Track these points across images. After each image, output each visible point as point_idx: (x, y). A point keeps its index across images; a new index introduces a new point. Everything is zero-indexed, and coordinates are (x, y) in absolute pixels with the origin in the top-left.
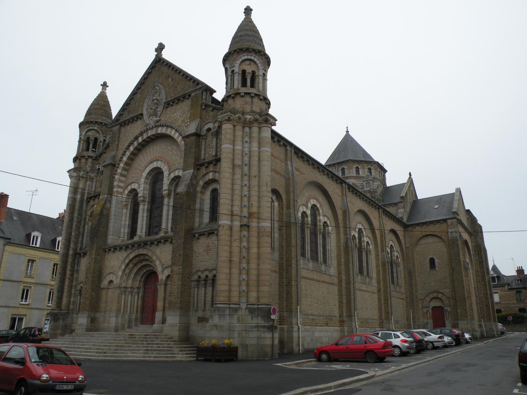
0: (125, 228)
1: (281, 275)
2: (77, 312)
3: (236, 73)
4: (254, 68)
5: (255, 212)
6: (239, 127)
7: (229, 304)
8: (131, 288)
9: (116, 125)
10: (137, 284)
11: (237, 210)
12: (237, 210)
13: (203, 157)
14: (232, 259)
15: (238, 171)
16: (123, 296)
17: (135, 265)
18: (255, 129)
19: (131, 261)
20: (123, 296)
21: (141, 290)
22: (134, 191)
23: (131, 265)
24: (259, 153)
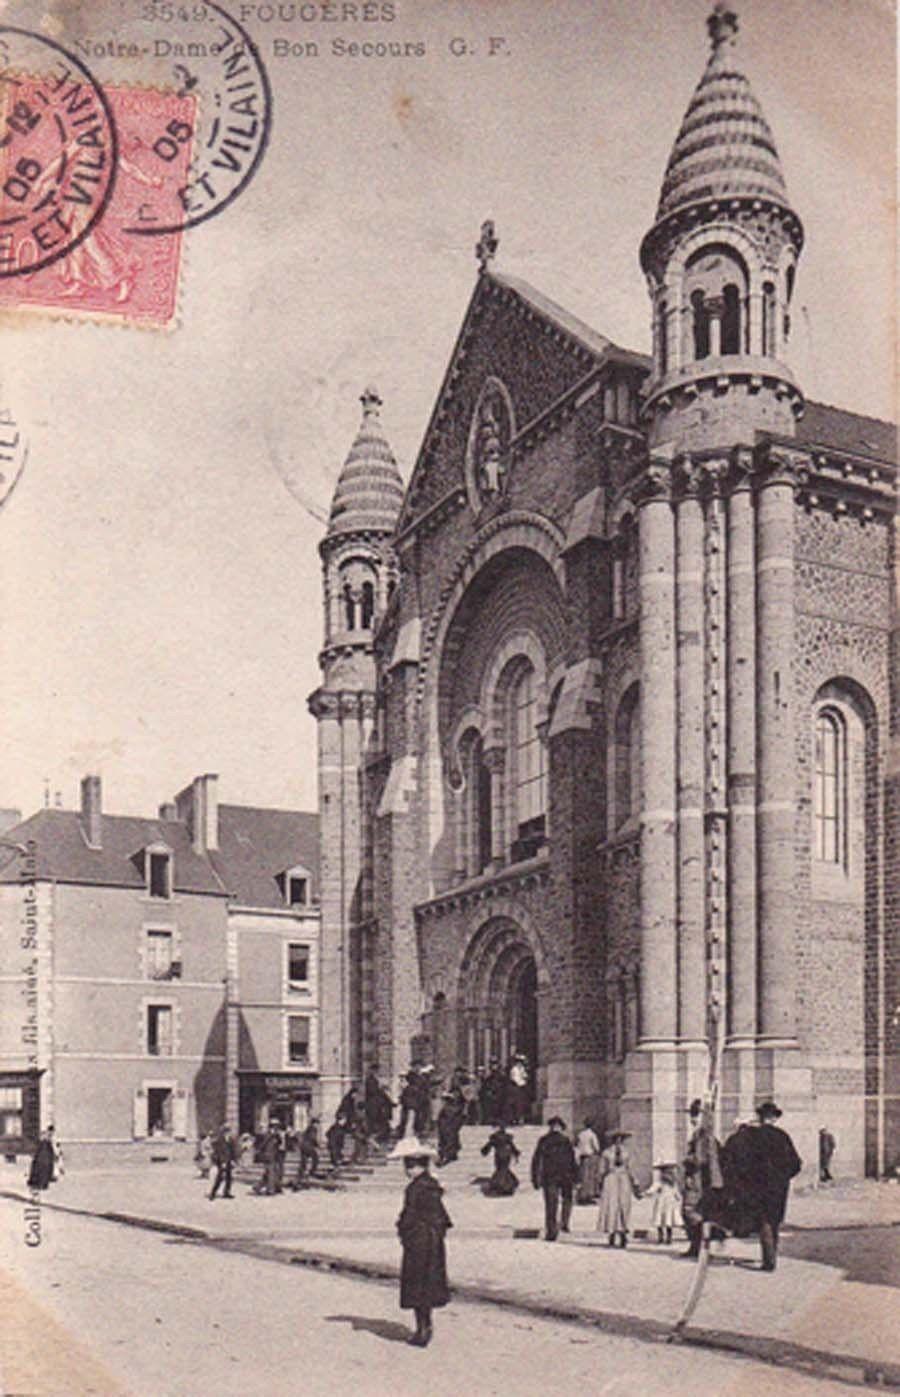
0: (464, 844)
1: (869, 948)
2: (618, 1058)
3: (673, 311)
4: (731, 274)
5: (745, 776)
6: (691, 507)
7: (678, 1043)
8: (487, 1009)
9: (407, 536)
10: (502, 996)
11: (693, 772)
12: (693, 772)
13: (618, 611)
14: (682, 918)
15: (694, 654)
16: (471, 1032)
17: (491, 948)
18: (742, 501)
19: (477, 937)
20: (471, 1032)
21: (516, 1010)
22: (472, 733)
23: (480, 950)
24: (757, 576)
